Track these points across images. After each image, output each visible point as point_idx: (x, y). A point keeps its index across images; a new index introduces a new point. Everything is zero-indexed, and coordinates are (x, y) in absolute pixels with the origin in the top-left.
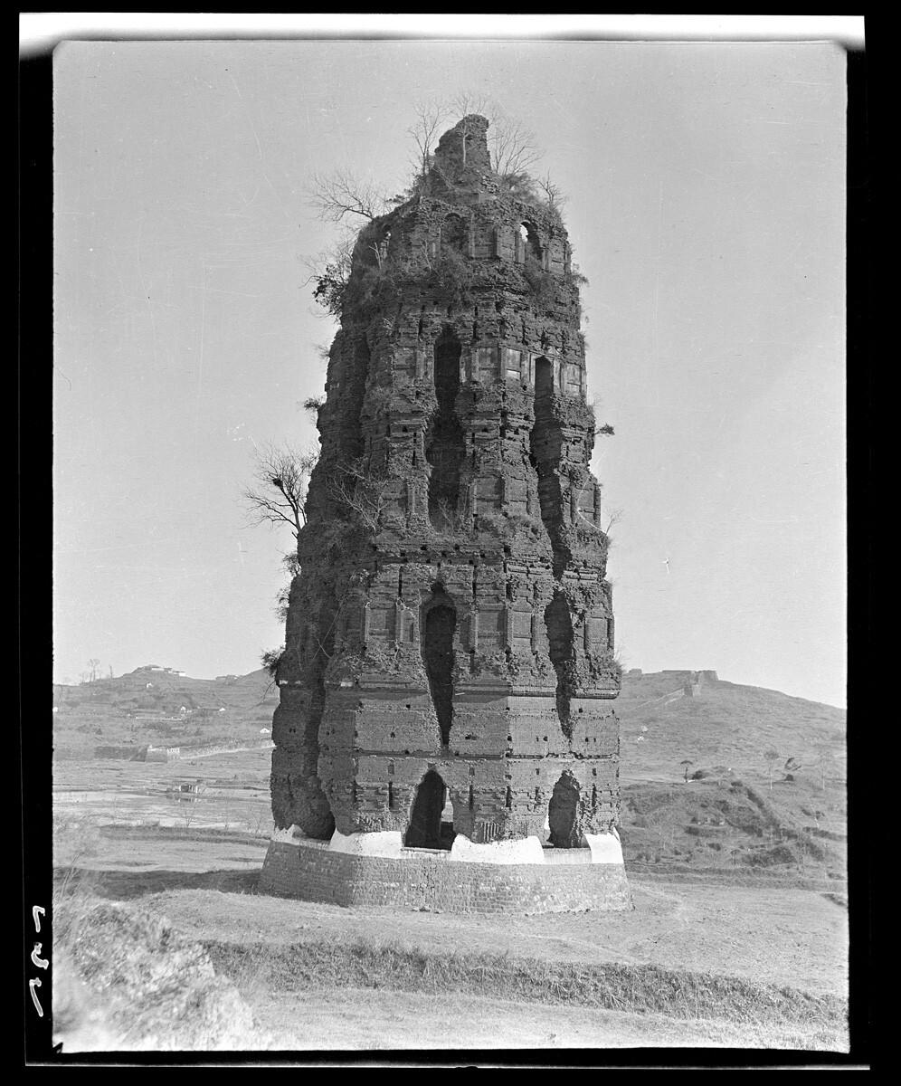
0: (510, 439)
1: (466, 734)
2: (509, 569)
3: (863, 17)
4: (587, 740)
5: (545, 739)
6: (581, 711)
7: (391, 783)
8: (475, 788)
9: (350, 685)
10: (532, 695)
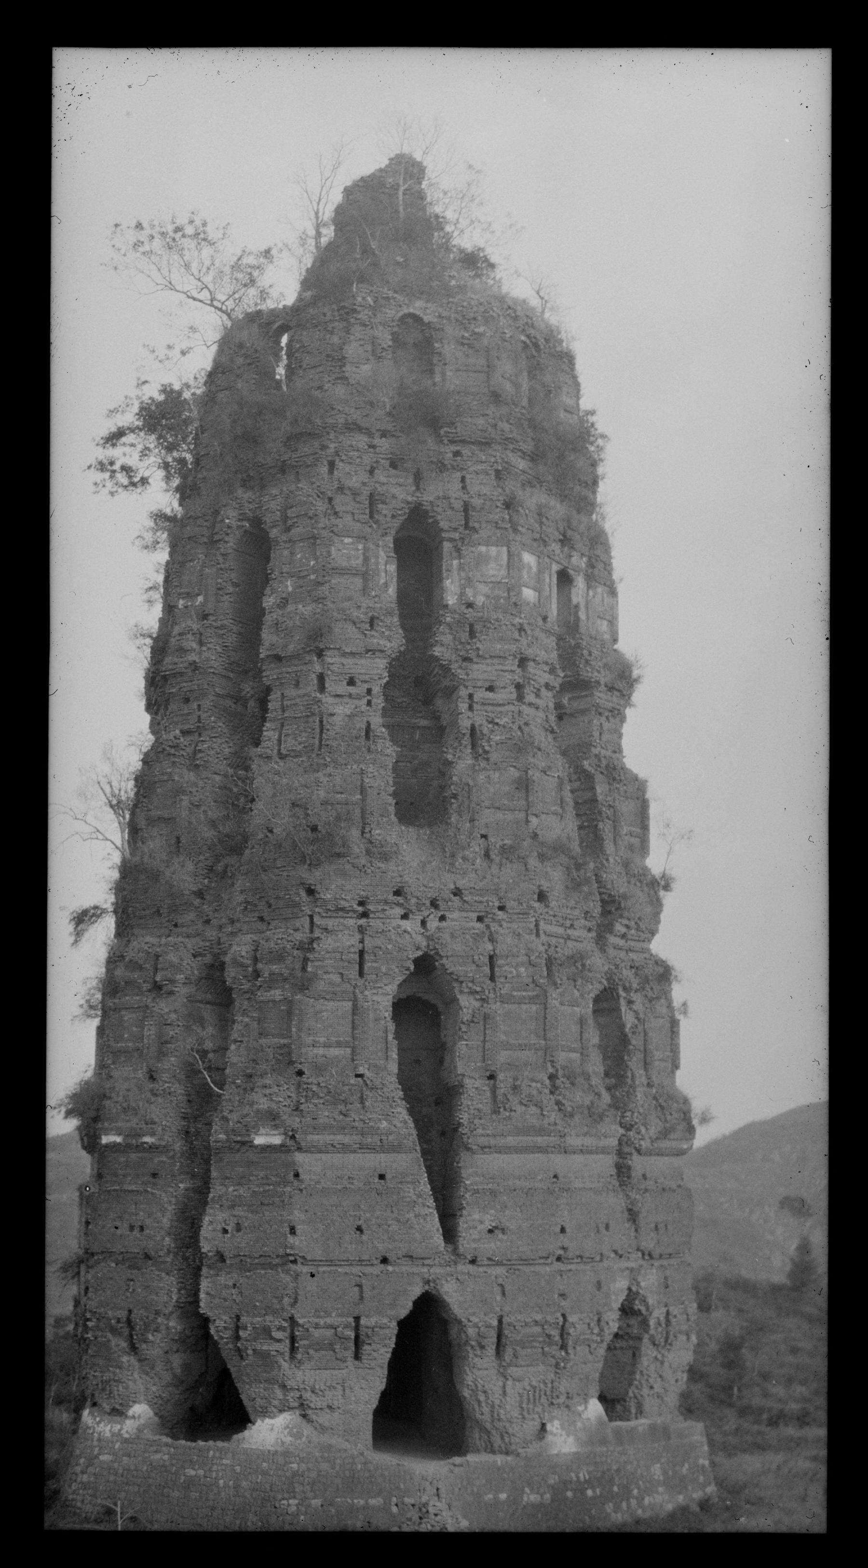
0: (530, 704)
1: (488, 1225)
2: (545, 933)
3: (778, 99)
4: (656, 1228)
5: (607, 1227)
6: (644, 1177)
7: (357, 1319)
8: (505, 1320)
9: (277, 1140)
10: (590, 1152)
